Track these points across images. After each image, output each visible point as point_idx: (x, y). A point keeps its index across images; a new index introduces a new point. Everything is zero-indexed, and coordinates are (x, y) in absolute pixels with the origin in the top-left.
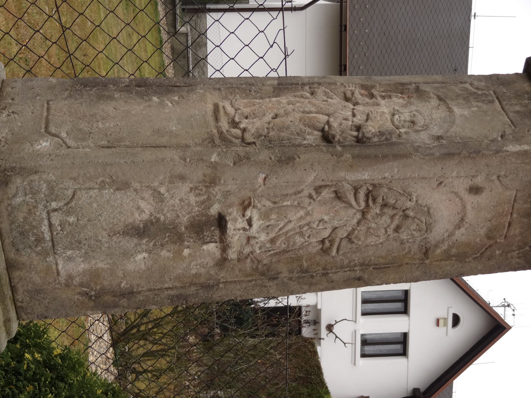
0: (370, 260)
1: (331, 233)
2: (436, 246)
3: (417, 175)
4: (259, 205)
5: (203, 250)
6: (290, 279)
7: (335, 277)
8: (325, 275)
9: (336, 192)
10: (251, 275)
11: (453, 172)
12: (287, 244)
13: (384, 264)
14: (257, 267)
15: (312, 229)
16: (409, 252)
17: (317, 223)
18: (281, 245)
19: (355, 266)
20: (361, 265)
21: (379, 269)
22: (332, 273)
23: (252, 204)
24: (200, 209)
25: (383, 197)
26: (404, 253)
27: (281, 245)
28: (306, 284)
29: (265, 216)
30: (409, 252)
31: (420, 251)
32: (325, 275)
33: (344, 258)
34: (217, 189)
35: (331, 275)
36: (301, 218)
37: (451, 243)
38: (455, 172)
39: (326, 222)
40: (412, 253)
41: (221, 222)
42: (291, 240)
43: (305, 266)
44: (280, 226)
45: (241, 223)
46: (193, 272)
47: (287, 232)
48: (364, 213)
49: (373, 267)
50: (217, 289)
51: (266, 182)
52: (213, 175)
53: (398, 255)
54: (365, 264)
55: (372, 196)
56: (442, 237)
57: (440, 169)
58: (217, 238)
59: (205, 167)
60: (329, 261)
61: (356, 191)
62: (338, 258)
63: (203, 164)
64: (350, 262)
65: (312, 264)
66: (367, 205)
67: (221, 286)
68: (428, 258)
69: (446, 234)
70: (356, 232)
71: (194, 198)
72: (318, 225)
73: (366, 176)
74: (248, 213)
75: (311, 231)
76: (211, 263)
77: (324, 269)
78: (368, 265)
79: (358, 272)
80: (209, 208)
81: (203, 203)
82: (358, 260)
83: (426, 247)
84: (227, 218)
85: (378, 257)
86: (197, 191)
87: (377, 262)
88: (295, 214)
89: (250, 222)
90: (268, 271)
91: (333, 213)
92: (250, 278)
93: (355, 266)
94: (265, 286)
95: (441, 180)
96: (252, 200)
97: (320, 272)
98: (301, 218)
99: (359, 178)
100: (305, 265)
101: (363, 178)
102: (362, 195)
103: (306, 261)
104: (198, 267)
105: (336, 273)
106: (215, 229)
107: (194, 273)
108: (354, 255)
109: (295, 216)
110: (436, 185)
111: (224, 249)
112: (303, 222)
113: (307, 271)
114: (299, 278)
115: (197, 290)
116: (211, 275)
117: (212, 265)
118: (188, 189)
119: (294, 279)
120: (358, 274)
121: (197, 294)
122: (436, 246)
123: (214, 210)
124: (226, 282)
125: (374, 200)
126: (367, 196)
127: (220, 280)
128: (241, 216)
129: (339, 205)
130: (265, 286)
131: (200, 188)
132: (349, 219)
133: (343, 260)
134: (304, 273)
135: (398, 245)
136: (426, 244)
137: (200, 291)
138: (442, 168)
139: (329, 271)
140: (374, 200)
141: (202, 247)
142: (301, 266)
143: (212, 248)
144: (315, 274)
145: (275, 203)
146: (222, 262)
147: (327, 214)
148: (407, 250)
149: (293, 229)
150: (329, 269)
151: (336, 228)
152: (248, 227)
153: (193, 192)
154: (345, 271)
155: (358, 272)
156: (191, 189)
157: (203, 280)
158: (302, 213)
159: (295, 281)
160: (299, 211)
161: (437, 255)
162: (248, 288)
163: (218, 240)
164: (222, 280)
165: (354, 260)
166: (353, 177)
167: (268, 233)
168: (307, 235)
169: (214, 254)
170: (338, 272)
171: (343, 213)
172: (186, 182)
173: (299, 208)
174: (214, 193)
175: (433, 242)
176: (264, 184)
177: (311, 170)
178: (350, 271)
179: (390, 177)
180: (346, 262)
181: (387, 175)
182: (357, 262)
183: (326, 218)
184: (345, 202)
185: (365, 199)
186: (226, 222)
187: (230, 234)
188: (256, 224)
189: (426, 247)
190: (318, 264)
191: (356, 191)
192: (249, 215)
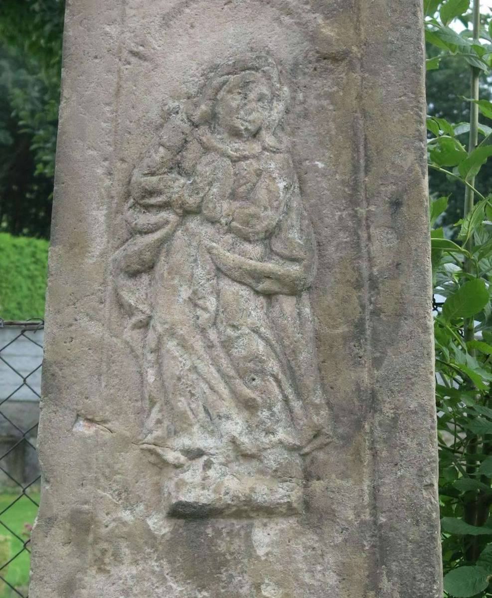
0: (343, 182)
1: (234, 280)
2: (313, 37)
3: (107, 108)
4: (158, 433)
5: (267, 554)
6: (377, 362)
7: (383, 261)
8: (374, 283)
9: (134, 274)
10: (358, 453)
11: (106, 34)
12: (253, 375)
13: (356, 150)
14: (342, 437)
15: (218, 321)
16: (330, 96)
17: (199, 312)
18: (256, 387)
19: (354, 216)
20: (353, 201)
21: (368, 160)
22: (371, 267)
23: (153, 447)
24: (155, 556)
25: (145, 175)
26: (331, 107)
27: (255, 388)
28: (398, 326)
29: (179, 423)
30: (330, 96)
31: (332, 71)
32: (374, 283)
33: (334, 243)
34: (104, 518)
35: (375, 269)
36: (183, 346)
37: (308, 7)
38: (108, 29)
39: (195, 293)
40: (335, 89)
41: (186, 514)
42: (241, 365)
43: (347, 329)
44: (208, 391)
45: (193, 474)
46: (332, 579)
47: (225, 377)
48: (187, 212)
49: (362, 174)
50: (391, 529)
51: (97, 419)
52: (68, 526)
53: (334, 121)
54: (351, 195)
55: (143, 197)
56: (295, 27)
57: (97, 61)
58: (237, 524)
59: (47, 540)
60: (338, 276)
61: (137, 232)
62: (334, 256)
63: (40, 544)
64: (345, 228)
65: (344, 315)
66: (166, 206)
67: (383, 519)
68: (346, 53)
69: (287, 20)
70: (234, 224)
71: (123, 568)
72: (205, 309)
73: (99, 215)
74: (171, 456)
75: (222, 322)
76: (311, 538)
77: (358, 285)
78: (355, 188)
79: (372, 208)
80: (154, 537)
81: (136, 549)
82: (340, 210)
83: (318, 61)
84: (174, 501)
85: (336, 165)
86: (107, 560)
87: (349, 167)
88: (174, 358)
89: (194, 454)
90: (351, 412)
91: (173, 279)
92: (367, 457)
93: (354, 216)
94: (395, 419)
95: (125, 54)
96: (145, 446)
97: (367, 296)
98: (184, 345)
99: (104, 227)
100: (343, 329)
101: (102, 219)
102: (144, 219)
103: (335, 327)
104: (319, 568)
105: (370, 259)
106: (213, 526)
107: (336, 577)
108: (327, 221)
109: (178, 361)
110: (146, 64)
111: (269, 511)
112: (198, 344)
113: (359, 326)
114: (375, 341)
115: (390, 574)
116: (346, 541)
117: (316, 538)
118: (101, 577)
119: (378, 355)
120: (378, 208)
121: (401, 576)
122: (313, 37)
123: (159, 525)
124: (375, 508)
125: (151, 193)
126: (148, 208)
127: (363, 523)
128: (178, 471)
129: (162, 267)
130: (395, 419)
131: (99, 554)
132: (194, 244)
133: (338, 245)
134: (363, 332)
135: (308, 123)
136: (310, 62)
137: (394, 568)
138: (96, 57)
139: (366, 274)
140: (151, 193)
141: (258, 558)
142: (345, 338)
143: (264, 536)
144: (371, 307)
145: (153, 403)
146: (311, 513)
147: (175, 290)
148: (325, 103)
149: (215, 362)
150: (356, 274)
151: (218, 269)
152: (205, 458)
153: (108, 568)
154: (369, 238)
155: (372, 208)
156: (100, 570)
157: (360, 560)
158: (171, 345)
159: (384, 353)
160: (168, 351)
161: (338, 34)
162: (397, 458)
163: (245, 522)
164: (367, 517)
165: (341, 218)
166: (98, 240)
167: (220, 417)
168: (230, 331)
169: (282, 531)
170: (369, 252)
171: (177, 258)
172: (81, 580)
173: (163, 351)
174: (112, 525)
175: (307, 45)
176: (104, 421)
177: (73, 327)
178: (368, 227)
179: (106, 164)
180: (344, 237)
181: (100, 171)
182: (345, 213)
183: (185, 293)
184: (157, 255)
185: (154, 210)
186: (181, 504)
187: (213, 496)
188: (198, 439)
189: (318, 61)
190: (345, 300)
191: (137, 232)
192: (178, 454)
